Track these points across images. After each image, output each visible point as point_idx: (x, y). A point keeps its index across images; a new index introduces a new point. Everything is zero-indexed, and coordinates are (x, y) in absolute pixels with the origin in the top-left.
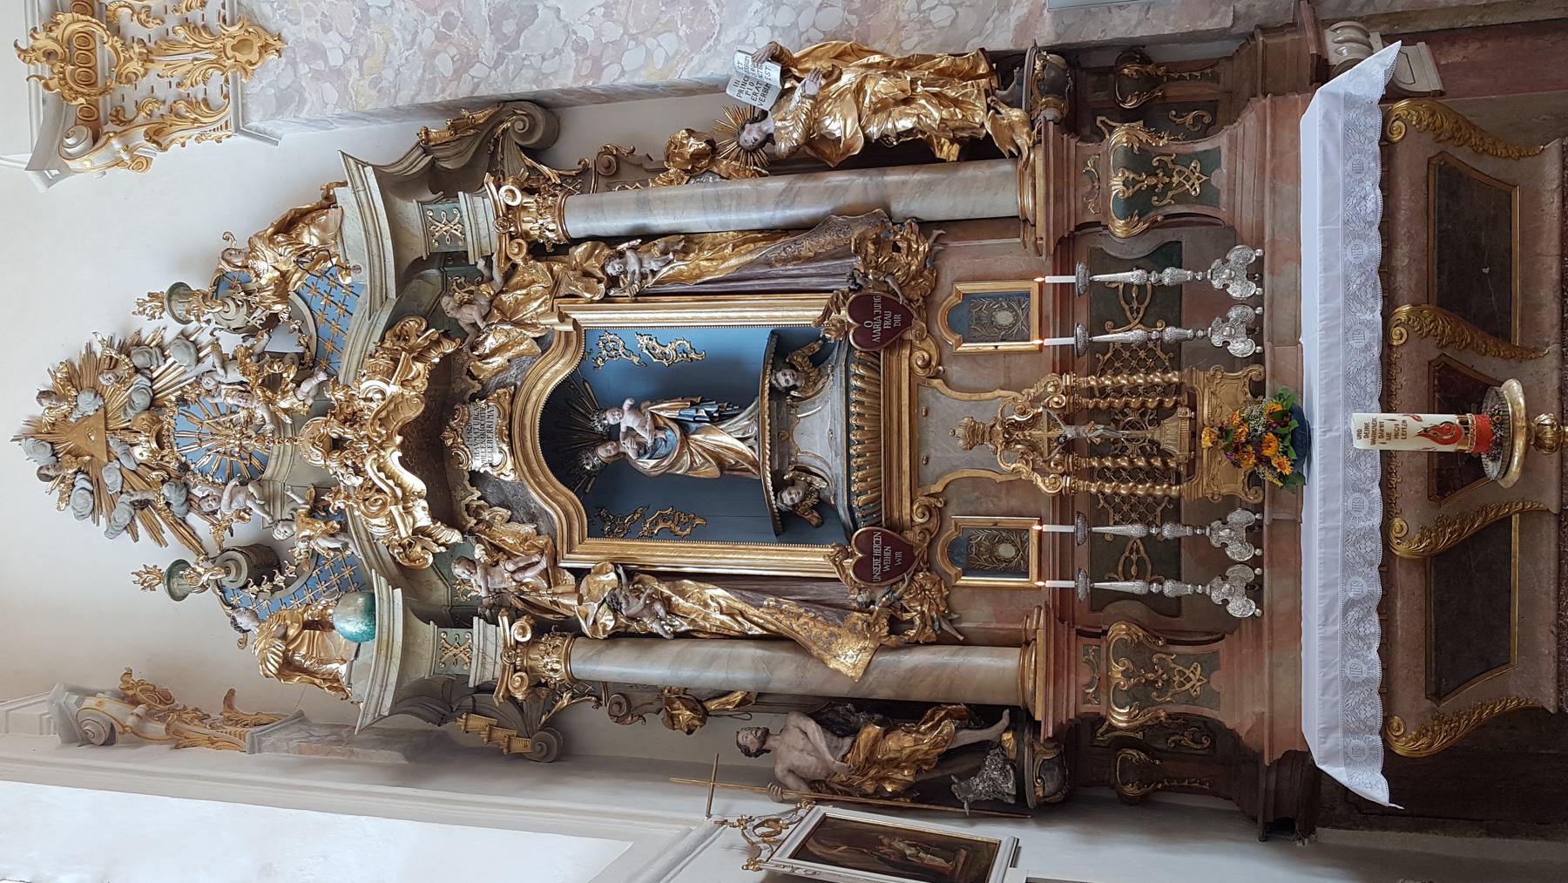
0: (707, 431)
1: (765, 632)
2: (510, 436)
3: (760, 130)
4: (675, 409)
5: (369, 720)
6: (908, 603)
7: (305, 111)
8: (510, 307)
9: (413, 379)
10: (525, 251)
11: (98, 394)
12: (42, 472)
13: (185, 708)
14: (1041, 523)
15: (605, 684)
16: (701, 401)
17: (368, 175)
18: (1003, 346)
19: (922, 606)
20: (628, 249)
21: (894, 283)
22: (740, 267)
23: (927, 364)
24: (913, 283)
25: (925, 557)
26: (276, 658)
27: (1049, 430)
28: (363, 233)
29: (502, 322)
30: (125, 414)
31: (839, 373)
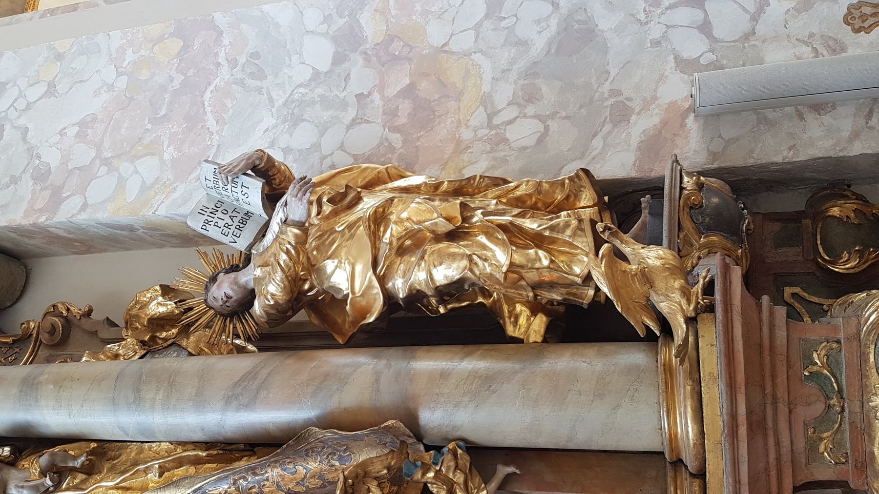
3: (236, 282)
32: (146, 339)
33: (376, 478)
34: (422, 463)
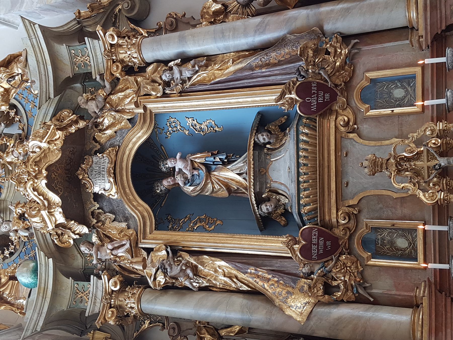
0: (221, 170)
1: (249, 289)
2: (114, 174)
4: (202, 158)
6: (336, 274)
7: (24, 7)
9: (56, 140)
14: (424, 224)
15: (167, 318)
16: (218, 153)
17: (37, 29)
18: (397, 110)
19: (344, 277)
21: (325, 75)
22: (236, 72)
23: (347, 124)
24: (337, 74)
25: (347, 245)
27: (428, 161)
28: (36, 62)
31: (293, 132)
32: (213, 20)
33: (310, 48)
34: (326, 42)
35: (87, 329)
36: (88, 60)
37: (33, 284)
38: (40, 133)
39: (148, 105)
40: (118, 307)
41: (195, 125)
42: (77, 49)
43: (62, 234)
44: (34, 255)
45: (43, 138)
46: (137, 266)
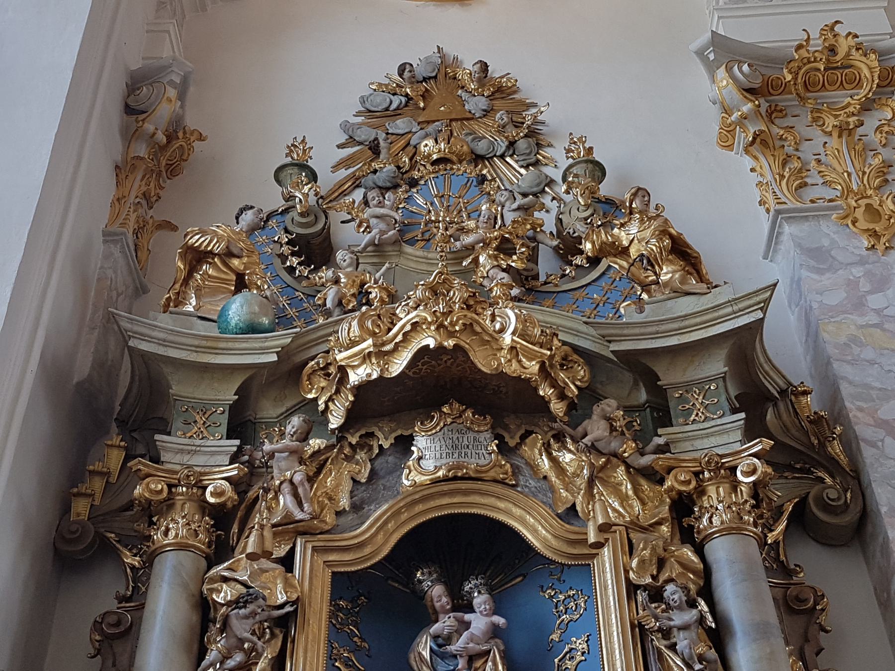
2: (455, 478)
5: (125, 324)
7: (809, 274)
8: (609, 477)
9: (520, 361)
10: (683, 488)
11: (487, 113)
12: (408, 66)
13: (162, 188)
15: (142, 606)
17: (753, 314)
20: (700, 611)
26: (205, 244)
28: (683, 313)
29: (592, 466)
30: (467, 135)
35: (131, 431)
36: (697, 418)
37: (227, 326)
38: (532, 329)
39: (608, 550)
40: (171, 502)
41: (573, 657)
42: (720, 396)
43: (329, 375)
44: (288, 316)
45: (521, 336)
46: (255, 540)
